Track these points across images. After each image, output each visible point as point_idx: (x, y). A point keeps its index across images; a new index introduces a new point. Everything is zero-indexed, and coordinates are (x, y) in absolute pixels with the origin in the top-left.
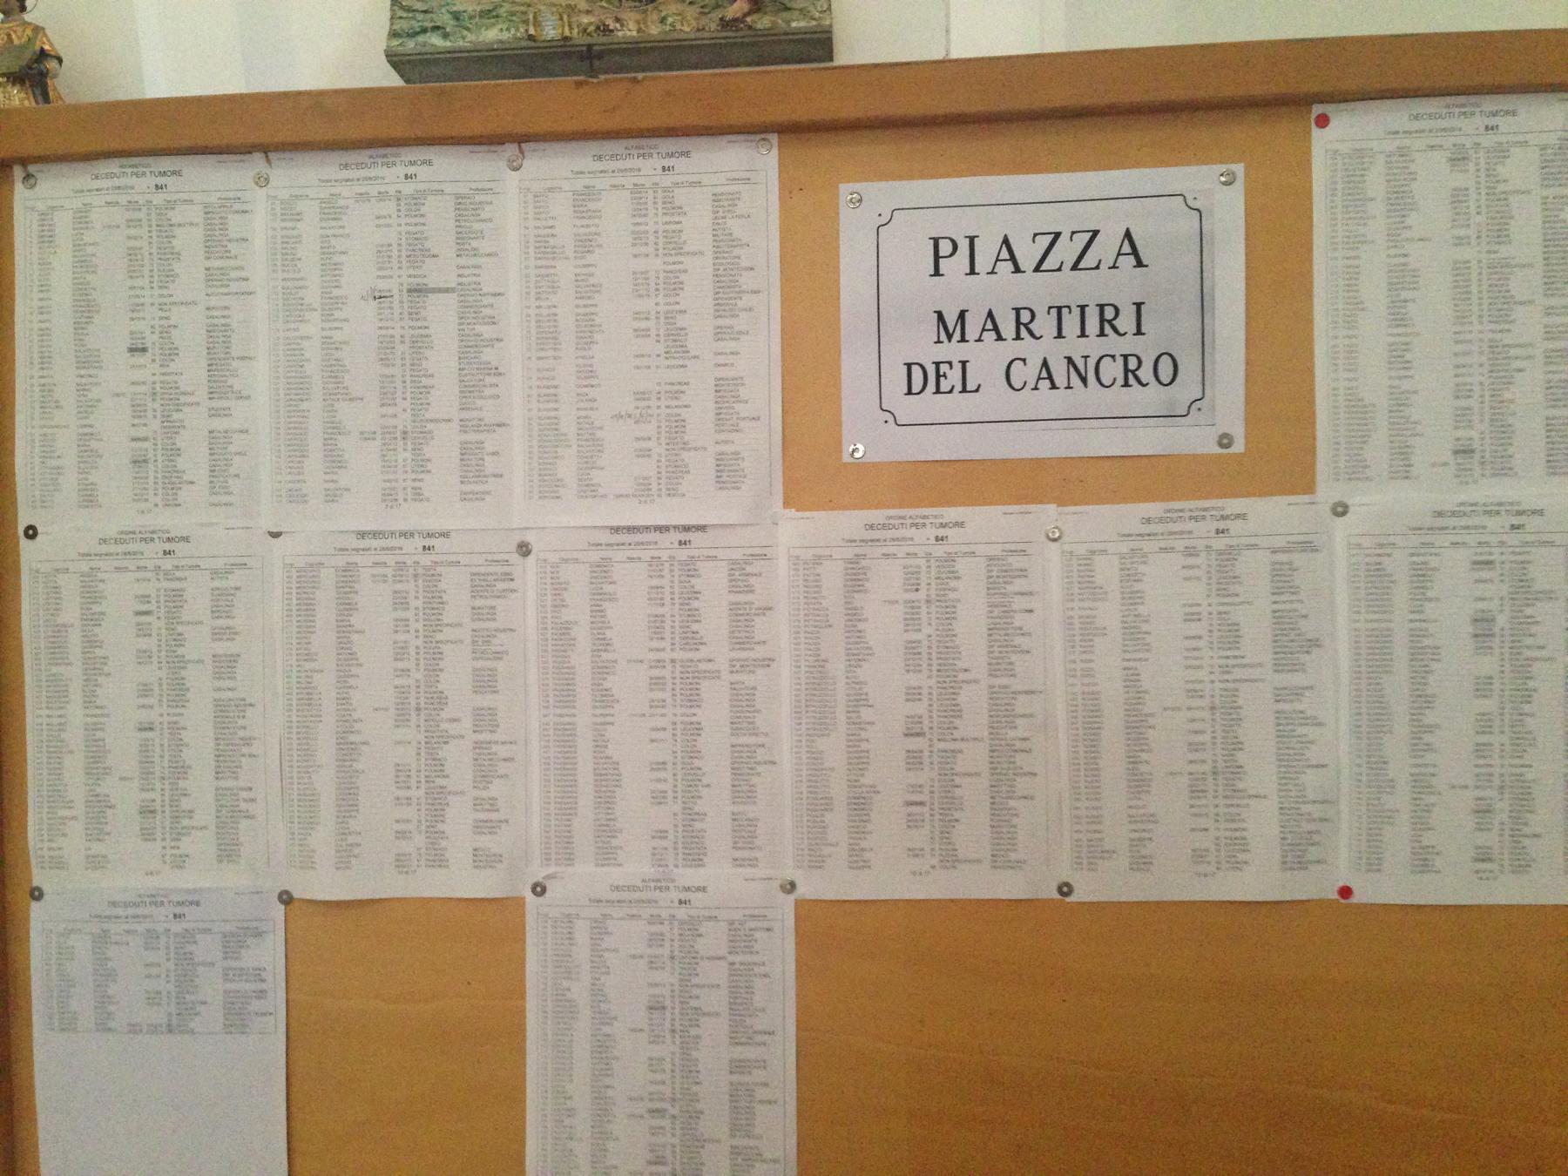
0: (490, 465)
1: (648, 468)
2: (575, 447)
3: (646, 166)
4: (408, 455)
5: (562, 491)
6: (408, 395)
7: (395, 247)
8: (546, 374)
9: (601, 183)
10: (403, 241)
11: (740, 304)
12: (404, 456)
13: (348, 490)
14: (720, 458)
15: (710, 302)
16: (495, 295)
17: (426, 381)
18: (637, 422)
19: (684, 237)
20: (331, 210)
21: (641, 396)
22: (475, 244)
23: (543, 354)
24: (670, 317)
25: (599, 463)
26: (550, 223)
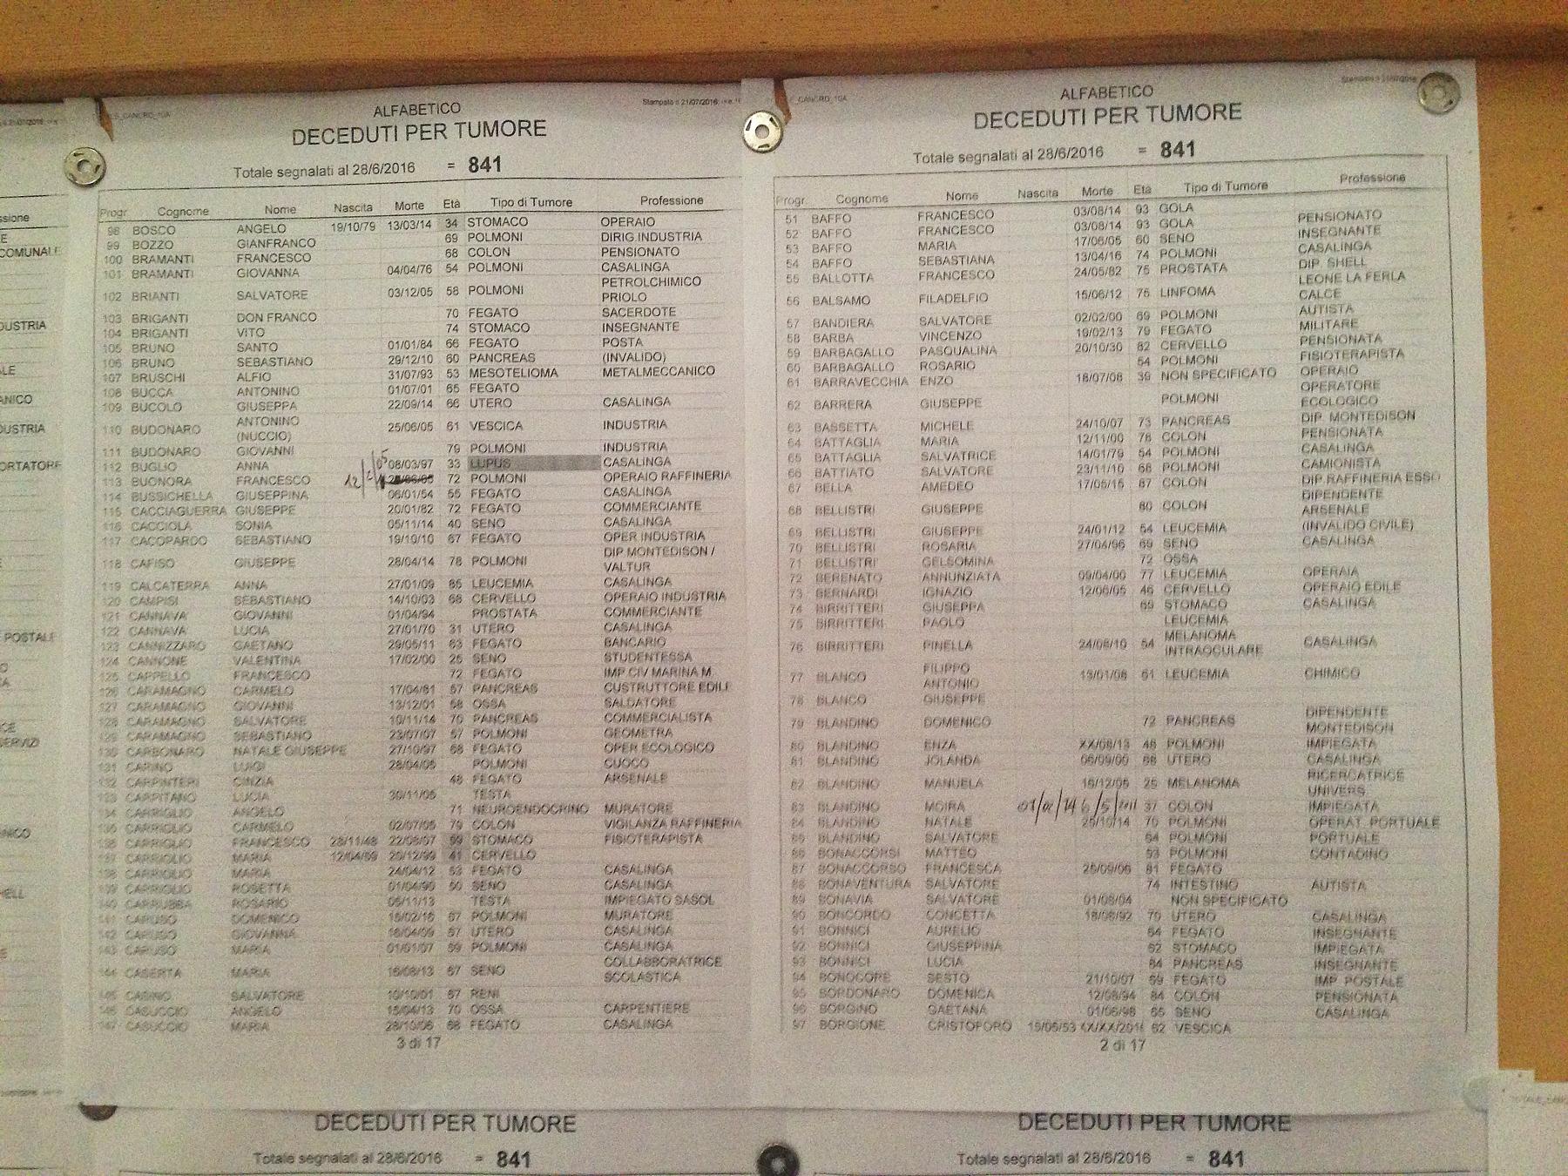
0: (687, 929)
1: (1121, 948)
2: (918, 883)
3: (1121, 142)
4: (464, 902)
5: (886, 1008)
6: (466, 737)
7: (440, 351)
8: (842, 689)
9: (987, 185)
10: (463, 336)
11: (1377, 509)
12: (453, 903)
13: (296, 995)
14: (1326, 931)
15: (1290, 506)
16: (704, 476)
17: (516, 704)
18: (1092, 822)
19: (1218, 330)
20: (270, 249)
21: (1097, 750)
22: (652, 341)
23: (835, 635)
24: (1180, 543)
25: (988, 931)
26: (857, 289)
